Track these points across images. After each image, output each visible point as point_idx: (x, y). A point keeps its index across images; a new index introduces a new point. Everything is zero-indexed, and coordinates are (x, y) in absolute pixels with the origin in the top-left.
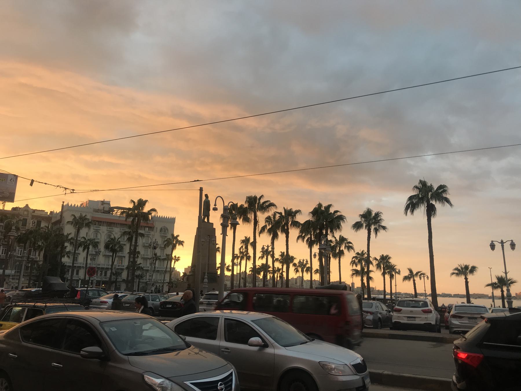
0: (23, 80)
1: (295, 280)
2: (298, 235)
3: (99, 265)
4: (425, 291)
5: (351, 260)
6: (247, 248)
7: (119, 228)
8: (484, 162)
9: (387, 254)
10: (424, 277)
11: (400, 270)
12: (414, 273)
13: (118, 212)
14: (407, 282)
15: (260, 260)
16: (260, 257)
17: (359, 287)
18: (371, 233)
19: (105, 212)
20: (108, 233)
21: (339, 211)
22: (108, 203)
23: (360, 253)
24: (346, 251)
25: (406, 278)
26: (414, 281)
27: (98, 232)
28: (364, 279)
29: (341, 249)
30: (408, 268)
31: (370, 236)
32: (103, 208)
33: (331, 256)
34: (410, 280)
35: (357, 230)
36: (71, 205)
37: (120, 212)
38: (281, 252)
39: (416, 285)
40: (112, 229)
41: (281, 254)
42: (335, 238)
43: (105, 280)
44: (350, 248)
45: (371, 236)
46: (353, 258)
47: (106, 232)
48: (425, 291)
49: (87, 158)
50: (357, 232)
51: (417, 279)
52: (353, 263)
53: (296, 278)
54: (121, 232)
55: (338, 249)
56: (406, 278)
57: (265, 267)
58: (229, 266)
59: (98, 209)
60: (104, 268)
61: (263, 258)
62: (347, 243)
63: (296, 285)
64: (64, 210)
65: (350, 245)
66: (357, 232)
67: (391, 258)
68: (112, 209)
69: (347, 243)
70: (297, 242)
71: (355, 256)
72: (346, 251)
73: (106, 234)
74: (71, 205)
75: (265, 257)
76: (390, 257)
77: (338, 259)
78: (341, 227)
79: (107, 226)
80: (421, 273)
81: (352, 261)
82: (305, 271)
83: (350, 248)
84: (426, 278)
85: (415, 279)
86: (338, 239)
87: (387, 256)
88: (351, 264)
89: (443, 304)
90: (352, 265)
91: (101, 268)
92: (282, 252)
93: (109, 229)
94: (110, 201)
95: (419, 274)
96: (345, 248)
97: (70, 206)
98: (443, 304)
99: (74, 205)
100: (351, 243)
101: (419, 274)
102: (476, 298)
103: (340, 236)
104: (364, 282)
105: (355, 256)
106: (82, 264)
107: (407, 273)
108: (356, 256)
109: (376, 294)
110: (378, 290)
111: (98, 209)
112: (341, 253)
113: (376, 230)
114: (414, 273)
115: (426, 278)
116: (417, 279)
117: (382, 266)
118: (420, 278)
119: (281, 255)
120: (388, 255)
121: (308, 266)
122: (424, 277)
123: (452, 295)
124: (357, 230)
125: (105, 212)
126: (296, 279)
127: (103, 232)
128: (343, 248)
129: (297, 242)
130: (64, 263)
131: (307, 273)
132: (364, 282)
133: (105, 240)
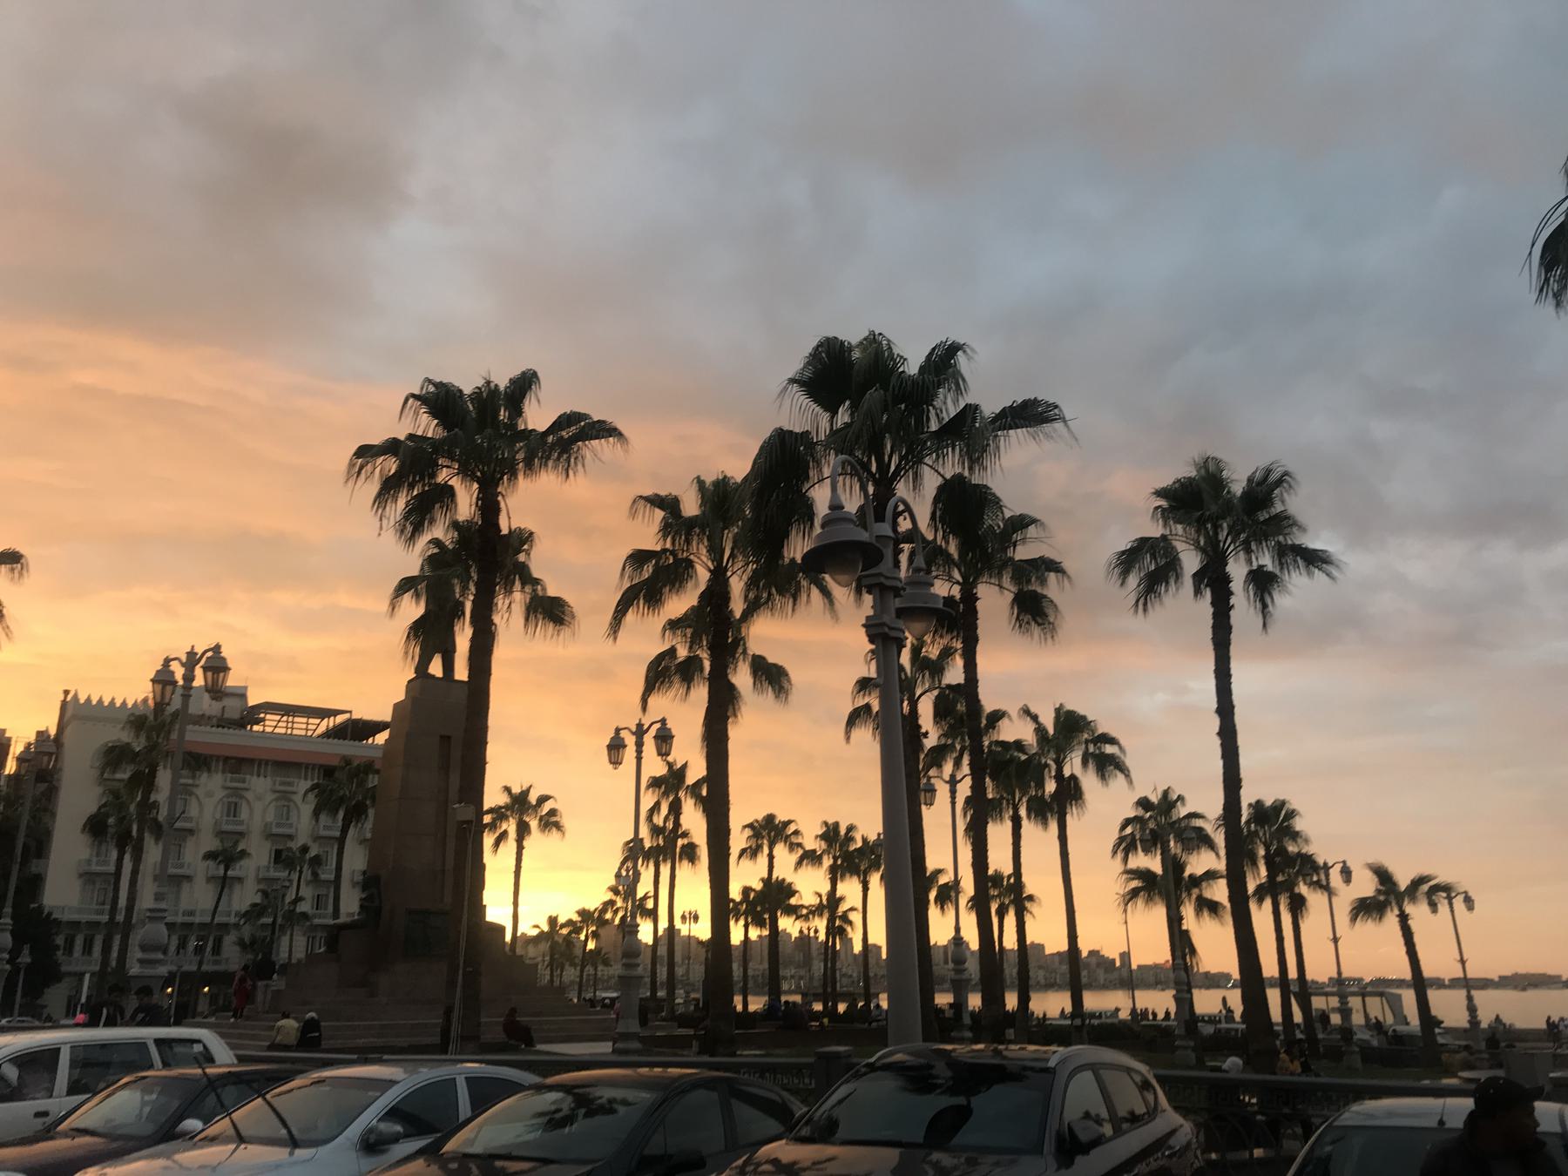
0: (86, 378)
1: (941, 951)
2: (851, 709)
3: (191, 913)
4: (1463, 962)
5: (1115, 835)
6: (676, 809)
7: (269, 779)
8: (1501, 553)
9: (1281, 798)
10: (1450, 899)
11: (1348, 864)
12: (1403, 883)
13: (275, 723)
14: (1367, 927)
15: (746, 863)
16: (743, 852)
17: (1156, 967)
18: (1232, 602)
19: (223, 723)
20: (227, 796)
21: (1034, 521)
22: (239, 692)
23: (1154, 799)
24: (1089, 782)
25: (1366, 908)
26: (1404, 919)
27: (191, 794)
28: (1183, 913)
29: (1067, 772)
30: (1370, 862)
31: (1229, 617)
32: (221, 711)
33: (1023, 812)
34: (1380, 918)
35: (1145, 604)
36: (88, 700)
37: (267, 723)
38: (826, 824)
39: (1416, 939)
40: (244, 782)
41: (824, 829)
42: (1035, 718)
43: (216, 968)
44: (1107, 764)
45: (1236, 617)
46: (1123, 827)
47: (220, 794)
48: (1463, 962)
49: (285, 598)
50: (1145, 610)
51: (1418, 912)
52: (1125, 846)
53: (946, 943)
54: (278, 792)
55: (1053, 774)
56: (1366, 908)
57: (774, 897)
58: (645, 898)
59: (201, 713)
60: (192, 924)
61: (759, 855)
62: (1092, 741)
63: (946, 966)
64: (69, 714)
65: (1109, 749)
66: (1145, 610)
67: (1298, 814)
68: (253, 715)
69: (1092, 741)
70: (848, 739)
71: (1132, 815)
72: (1089, 782)
73: (218, 802)
74: (88, 700)
75: (766, 850)
76: (1293, 811)
77: (1054, 826)
78: (1050, 611)
79: (224, 772)
80: (1432, 883)
81: (1121, 839)
82: (936, 902)
83: (1107, 764)
84: (1459, 903)
85: (1409, 909)
86: (1048, 722)
87: (1279, 806)
88: (1115, 853)
89: (1498, 1017)
90: (1120, 855)
91: (199, 924)
92: (831, 821)
93: (232, 780)
94: (246, 688)
95: (1425, 887)
96: (1085, 763)
97: (82, 701)
98: (1498, 1017)
99: (110, 700)
100: (1112, 741)
101: (1425, 887)
102: (1524, 989)
103: (1058, 711)
104: (1184, 927)
105: (1132, 816)
106: (180, 915)
107: (1365, 885)
108: (1136, 818)
109: (1200, 984)
110: (1207, 974)
111: (199, 716)
112: (1070, 792)
113: (1263, 583)
114: (1403, 883)
115: (1459, 903)
116: (1418, 912)
117: (1262, 852)
118: (1433, 906)
119: (824, 837)
120: (1283, 803)
121: (943, 880)
122: (1450, 899)
123: (1444, 980)
124: (1145, 604)
125: (223, 723)
126: (945, 947)
127: (210, 794)
128: (1073, 765)
129: (848, 739)
130: (50, 914)
131: (942, 908)
132: (1184, 927)
133: (216, 823)
